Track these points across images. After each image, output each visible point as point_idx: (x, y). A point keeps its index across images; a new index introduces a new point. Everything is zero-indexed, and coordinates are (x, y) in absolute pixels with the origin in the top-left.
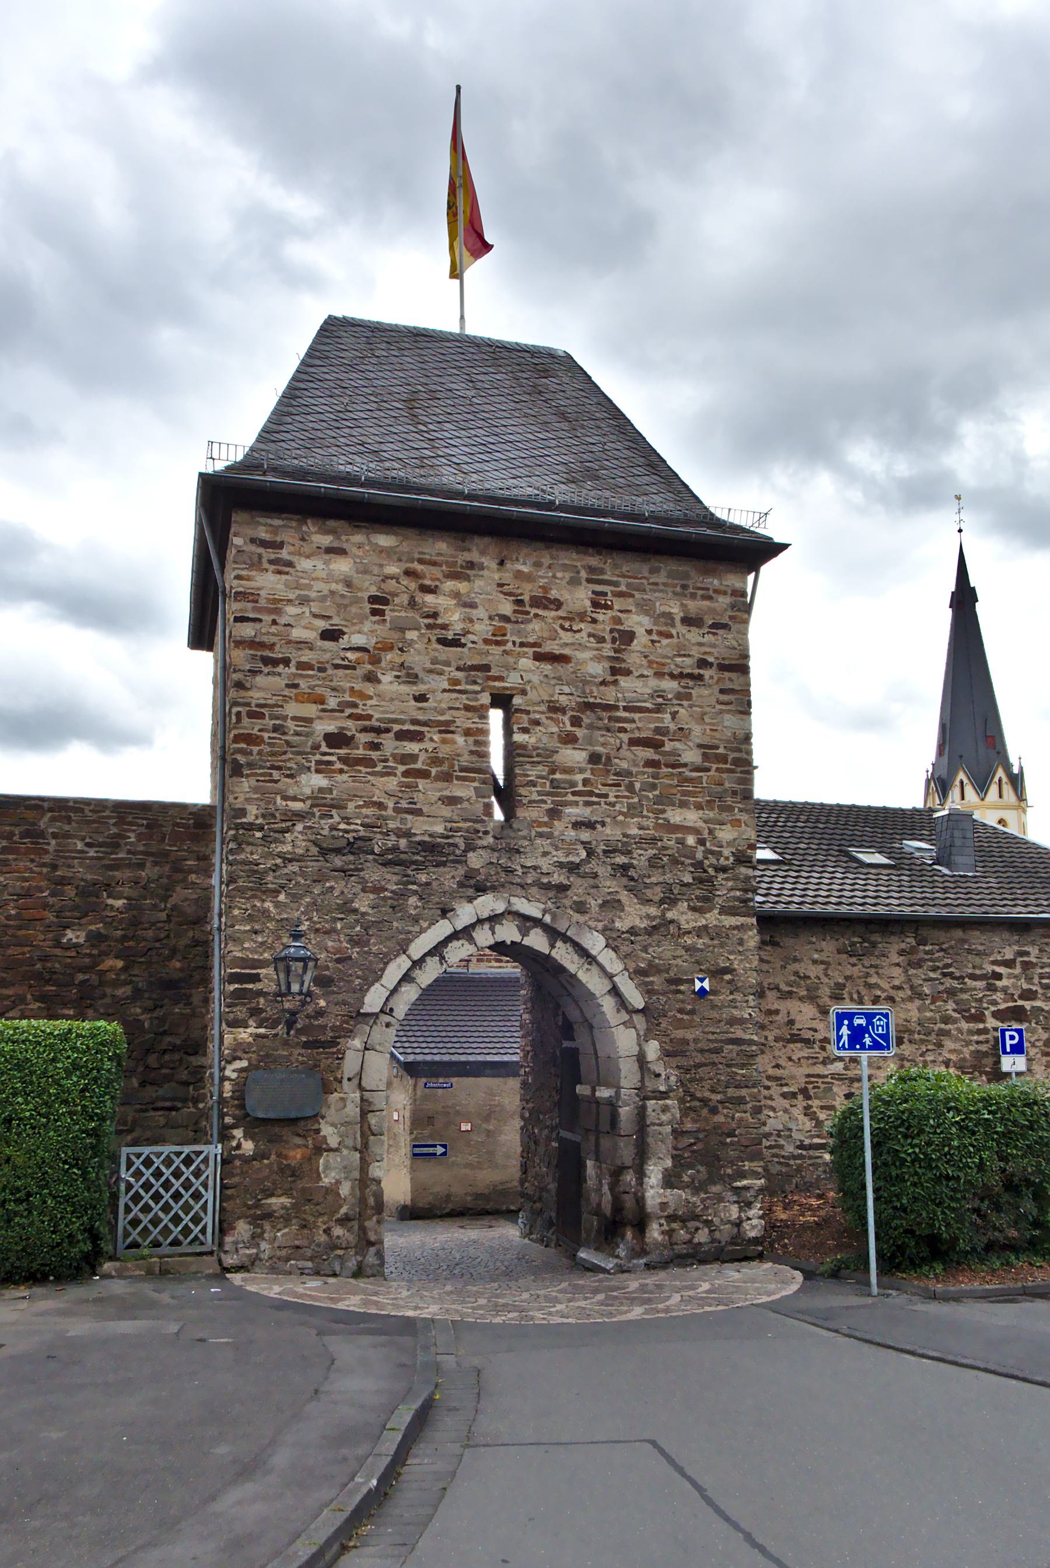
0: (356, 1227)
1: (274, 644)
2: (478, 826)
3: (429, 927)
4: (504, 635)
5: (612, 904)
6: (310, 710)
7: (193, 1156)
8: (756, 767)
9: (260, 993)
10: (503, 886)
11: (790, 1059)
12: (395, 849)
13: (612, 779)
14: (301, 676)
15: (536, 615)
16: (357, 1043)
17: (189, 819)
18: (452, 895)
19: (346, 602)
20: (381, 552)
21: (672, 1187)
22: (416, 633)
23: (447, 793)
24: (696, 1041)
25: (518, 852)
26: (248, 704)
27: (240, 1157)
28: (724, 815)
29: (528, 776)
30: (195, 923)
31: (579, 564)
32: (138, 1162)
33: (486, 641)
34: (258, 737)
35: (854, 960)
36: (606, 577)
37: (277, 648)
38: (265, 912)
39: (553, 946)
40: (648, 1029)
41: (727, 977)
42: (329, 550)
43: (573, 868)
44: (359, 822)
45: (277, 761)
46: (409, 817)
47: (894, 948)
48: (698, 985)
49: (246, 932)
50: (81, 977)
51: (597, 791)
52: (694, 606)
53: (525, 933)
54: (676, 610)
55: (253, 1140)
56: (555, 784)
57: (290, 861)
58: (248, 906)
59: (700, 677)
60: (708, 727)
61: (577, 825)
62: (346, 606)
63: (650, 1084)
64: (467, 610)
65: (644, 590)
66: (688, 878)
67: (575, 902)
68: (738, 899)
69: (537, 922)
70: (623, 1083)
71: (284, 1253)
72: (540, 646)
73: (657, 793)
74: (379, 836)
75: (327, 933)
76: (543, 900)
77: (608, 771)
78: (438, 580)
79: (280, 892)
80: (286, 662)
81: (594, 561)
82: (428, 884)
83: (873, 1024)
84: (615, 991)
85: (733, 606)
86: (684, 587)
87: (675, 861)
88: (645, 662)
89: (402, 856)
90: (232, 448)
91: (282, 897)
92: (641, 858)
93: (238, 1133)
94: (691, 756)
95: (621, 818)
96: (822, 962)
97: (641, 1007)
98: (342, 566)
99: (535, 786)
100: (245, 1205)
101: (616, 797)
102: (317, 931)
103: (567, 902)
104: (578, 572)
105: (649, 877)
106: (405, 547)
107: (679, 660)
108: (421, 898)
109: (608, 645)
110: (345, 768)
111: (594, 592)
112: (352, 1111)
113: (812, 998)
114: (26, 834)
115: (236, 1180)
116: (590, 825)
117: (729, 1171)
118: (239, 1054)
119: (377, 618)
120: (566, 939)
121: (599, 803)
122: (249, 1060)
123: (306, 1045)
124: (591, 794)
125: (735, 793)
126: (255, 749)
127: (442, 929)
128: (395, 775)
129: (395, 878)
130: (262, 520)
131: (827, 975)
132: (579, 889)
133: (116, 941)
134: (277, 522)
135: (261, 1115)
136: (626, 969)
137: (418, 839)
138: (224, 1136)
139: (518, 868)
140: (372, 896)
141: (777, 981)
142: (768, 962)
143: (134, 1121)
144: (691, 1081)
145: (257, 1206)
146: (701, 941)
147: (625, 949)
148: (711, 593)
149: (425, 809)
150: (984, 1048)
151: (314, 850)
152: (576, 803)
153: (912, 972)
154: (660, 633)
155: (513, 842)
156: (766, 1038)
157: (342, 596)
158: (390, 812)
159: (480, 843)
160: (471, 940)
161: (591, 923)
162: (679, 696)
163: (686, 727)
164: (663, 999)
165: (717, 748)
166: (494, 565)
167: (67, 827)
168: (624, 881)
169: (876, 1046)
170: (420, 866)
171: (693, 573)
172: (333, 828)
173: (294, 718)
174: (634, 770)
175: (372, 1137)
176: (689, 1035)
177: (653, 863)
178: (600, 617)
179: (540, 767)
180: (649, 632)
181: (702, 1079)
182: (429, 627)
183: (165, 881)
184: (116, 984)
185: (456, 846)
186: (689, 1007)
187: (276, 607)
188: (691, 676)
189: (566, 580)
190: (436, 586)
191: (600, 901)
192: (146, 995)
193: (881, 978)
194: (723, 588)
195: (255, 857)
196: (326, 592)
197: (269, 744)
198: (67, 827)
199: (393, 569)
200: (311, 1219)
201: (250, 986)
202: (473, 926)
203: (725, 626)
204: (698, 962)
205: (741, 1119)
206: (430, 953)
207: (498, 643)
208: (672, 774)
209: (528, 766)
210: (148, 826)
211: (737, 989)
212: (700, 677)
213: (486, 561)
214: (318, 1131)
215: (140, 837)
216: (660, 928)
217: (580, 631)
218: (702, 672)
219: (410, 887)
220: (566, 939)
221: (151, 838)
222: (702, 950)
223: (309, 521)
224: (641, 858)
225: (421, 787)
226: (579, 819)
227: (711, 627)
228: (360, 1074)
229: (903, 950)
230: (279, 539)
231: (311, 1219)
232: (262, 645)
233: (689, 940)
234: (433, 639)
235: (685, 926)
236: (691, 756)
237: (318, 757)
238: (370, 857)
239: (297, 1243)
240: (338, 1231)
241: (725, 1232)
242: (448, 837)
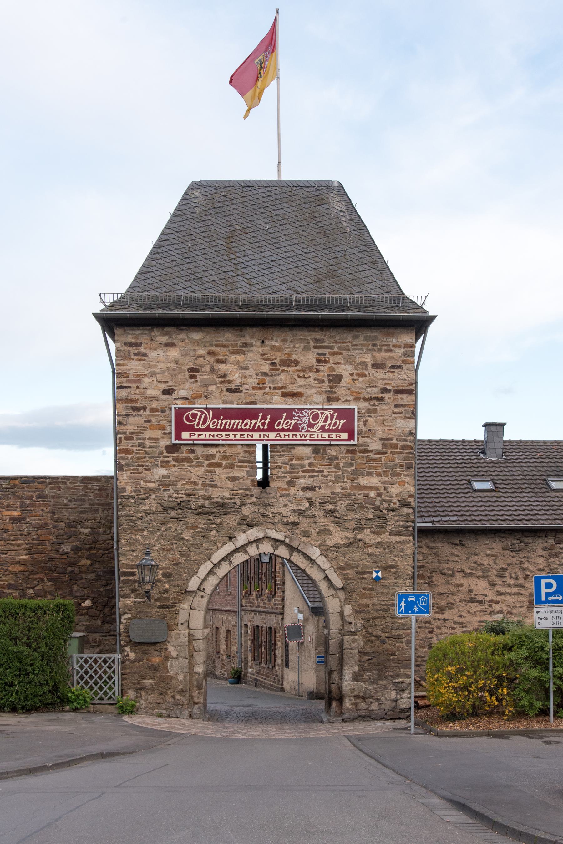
0: (188, 695)
1: (138, 400)
2: (248, 492)
3: (222, 546)
4: (264, 384)
5: (324, 532)
6: (158, 434)
7: (108, 659)
8: (494, 428)
10: (262, 524)
11: (469, 612)
12: (203, 506)
13: (326, 461)
14: (152, 415)
15: (283, 371)
16: (186, 606)
18: (234, 529)
20: (194, 343)
21: (357, 681)
22: (214, 387)
23: (231, 475)
24: (373, 605)
25: (269, 505)
26: (125, 433)
27: (128, 660)
28: (395, 479)
29: (277, 463)
31: (309, 338)
32: (82, 661)
33: (254, 388)
34: (131, 450)
35: (513, 554)
36: (326, 344)
37: (139, 402)
38: (137, 540)
39: (291, 555)
40: (346, 599)
41: (393, 570)
42: (166, 345)
43: (301, 513)
44: (183, 492)
46: (210, 489)
47: (539, 546)
48: (375, 575)
49: (128, 551)
50: (70, 569)
51: (317, 469)
52: (379, 356)
53: (275, 549)
54: (369, 360)
55: (134, 652)
56: (293, 467)
57: (149, 514)
58: (128, 537)
59: (382, 399)
60: (386, 428)
61: (304, 489)
62: (176, 375)
63: (346, 628)
64: (243, 371)
65: (349, 350)
66: (370, 516)
67: (303, 531)
68: (402, 526)
69: (282, 542)
70: (332, 627)
72: (285, 388)
73: (354, 468)
74: (194, 500)
75: (169, 550)
76: (285, 530)
77: (324, 458)
78: (227, 355)
79: (144, 530)
80: (144, 408)
82: (221, 524)
83: (419, 601)
84: (326, 578)
85: (405, 354)
86: (374, 345)
87: (362, 507)
88: (348, 393)
89: (207, 510)
90: (111, 295)
91: (145, 533)
92: (342, 506)
93: (128, 649)
94: (376, 445)
95: (331, 484)
96: (492, 556)
97: (341, 587)
98: (174, 353)
99: (280, 468)
100: (132, 683)
101: (328, 472)
102: (163, 549)
103: (298, 531)
104: (309, 343)
105: (347, 516)
106: (208, 339)
107: (369, 389)
108: (218, 532)
109: (326, 384)
110: (176, 464)
111: (318, 354)
112: (184, 639)
113: (485, 576)
114: (39, 497)
115: (128, 671)
116: (312, 489)
117: (391, 674)
119: (193, 380)
120: (299, 551)
121: (318, 476)
122: (132, 614)
123: (159, 607)
124: (313, 471)
125: (402, 466)
126: (129, 456)
128: (203, 466)
129: (203, 521)
130: (129, 332)
131: (495, 563)
132: (305, 523)
133: (86, 550)
134: (138, 332)
136: (332, 567)
137: (215, 500)
138: (122, 651)
139: (270, 514)
140: (191, 531)
141: (464, 566)
142: (458, 556)
143: (100, 641)
144: (369, 626)
146: (378, 550)
147: (332, 555)
148: (391, 347)
149: (219, 484)
151: (161, 508)
152: (304, 477)
153: (551, 560)
154: (358, 375)
155: (266, 500)
156: (455, 600)
157: (174, 370)
158: (200, 487)
159: (248, 501)
160: (246, 552)
161: (312, 542)
162: (369, 411)
163: (372, 429)
164: (354, 582)
165: (392, 440)
166: (258, 343)
167: (58, 492)
168: (332, 519)
169: (420, 611)
170: (216, 515)
171: (380, 337)
172: (170, 496)
174: (340, 456)
175: (195, 653)
176: (369, 602)
177: (349, 508)
178: (321, 368)
179: (284, 458)
180: (351, 374)
181: (376, 625)
182: (221, 383)
184: (86, 572)
186: (370, 587)
187: (138, 379)
188: (377, 399)
189: (302, 349)
190: (226, 359)
191: (317, 530)
192: (103, 578)
193: (531, 564)
194: (399, 344)
195: (131, 513)
196: (165, 368)
197: (137, 453)
198: (58, 492)
199: (202, 352)
200: (165, 690)
201: (131, 578)
202: (247, 545)
203: (399, 367)
204: (376, 562)
205: (399, 647)
206: (223, 559)
207: (260, 389)
208: (363, 457)
209: (277, 458)
211: (399, 577)
212: (382, 399)
213: (254, 342)
214: (166, 649)
215: (96, 496)
217: (309, 377)
218: (383, 395)
219: (211, 526)
220: (299, 551)
222: (378, 556)
224: (342, 506)
225: (217, 472)
226: (306, 486)
227: (390, 368)
228: (188, 621)
229: (546, 548)
230: (139, 341)
231: (165, 690)
232: (132, 400)
233: (370, 550)
234: (224, 389)
235: (368, 542)
236: (376, 445)
237: (162, 459)
238: (190, 511)
239: (158, 701)
240: (178, 697)
241: (388, 705)
242: (231, 499)
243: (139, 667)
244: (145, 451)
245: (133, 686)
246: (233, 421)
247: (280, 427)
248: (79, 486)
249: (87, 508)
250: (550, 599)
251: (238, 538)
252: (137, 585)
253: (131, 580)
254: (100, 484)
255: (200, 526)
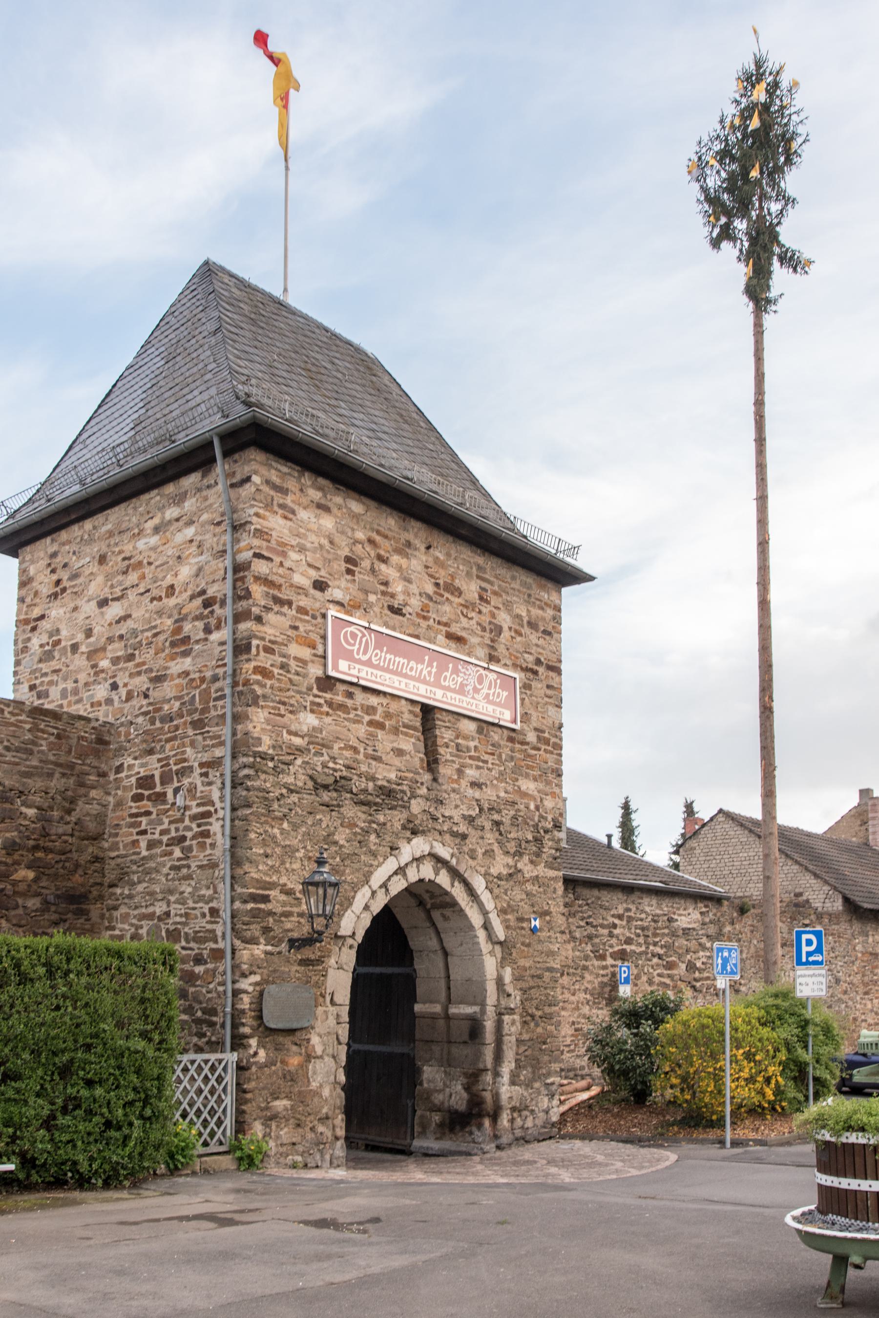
1: (280, 586)
6: (305, 653)
9: (271, 913)
12: (365, 791)
15: (447, 599)
17: (91, 734)
19: (330, 557)
23: (395, 745)
26: (263, 639)
27: (255, 1063)
30: (95, 839)
36: (487, 576)
42: (319, 506)
43: (470, 820)
44: (341, 762)
45: (282, 696)
46: (374, 763)
49: (260, 855)
57: (292, 791)
58: (261, 831)
71: (284, 1149)
80: (290, 603)
81: (480, 560)
82: (384, 824)
84: (487, 926)
89: (370, 797)
91: (285, 825)
92: (506, 817)
98: (328, 523)
108: (378, 836)
110: (331, 711)
118: (254, 969)
122: (262, 974)
126: (269, 683)
127: (391, 865)
129: (363, 816)
133: (28, 850)
134: (285, 469)
135: (273, 1026)
137: (380, 783)
138: (238, 1043)
140: (347, 831)
145: (267, 1108)
150: (605, 979)
151: (310, 784)
153: (571, 920)
157: (328, 552)
161: (479, 869)
170: (379, 808)
173: (295, 658)
178: (484, 610)
183: (70, 793)
184: (24, 895)
185: (404, 792)
187: (282, 549)
195: (268, 785)
197: (278, 679)
199: (360, 535)
201: (262, 906)
210: (59, 737)
214: (308, 1040)
216: (514, 875)
217: (472, 619)
221: (59, 749)
223: (306, 474)
231: (303, 1118)
237: (311, 698)
238: (348, 795)
239: (294, 1140)
242: (399, 785)
243: (270, 1076)
244: (290, 680)
245: (260, 1114)
246: (397, 659)
247: (447, 684)
248: (25, 722)
249: (36, 767)
250: (811, 959)
251: (403, 850)
252: (271, 920)
253: (264, 910)
254: (60, 725)
255: (359, 823)
